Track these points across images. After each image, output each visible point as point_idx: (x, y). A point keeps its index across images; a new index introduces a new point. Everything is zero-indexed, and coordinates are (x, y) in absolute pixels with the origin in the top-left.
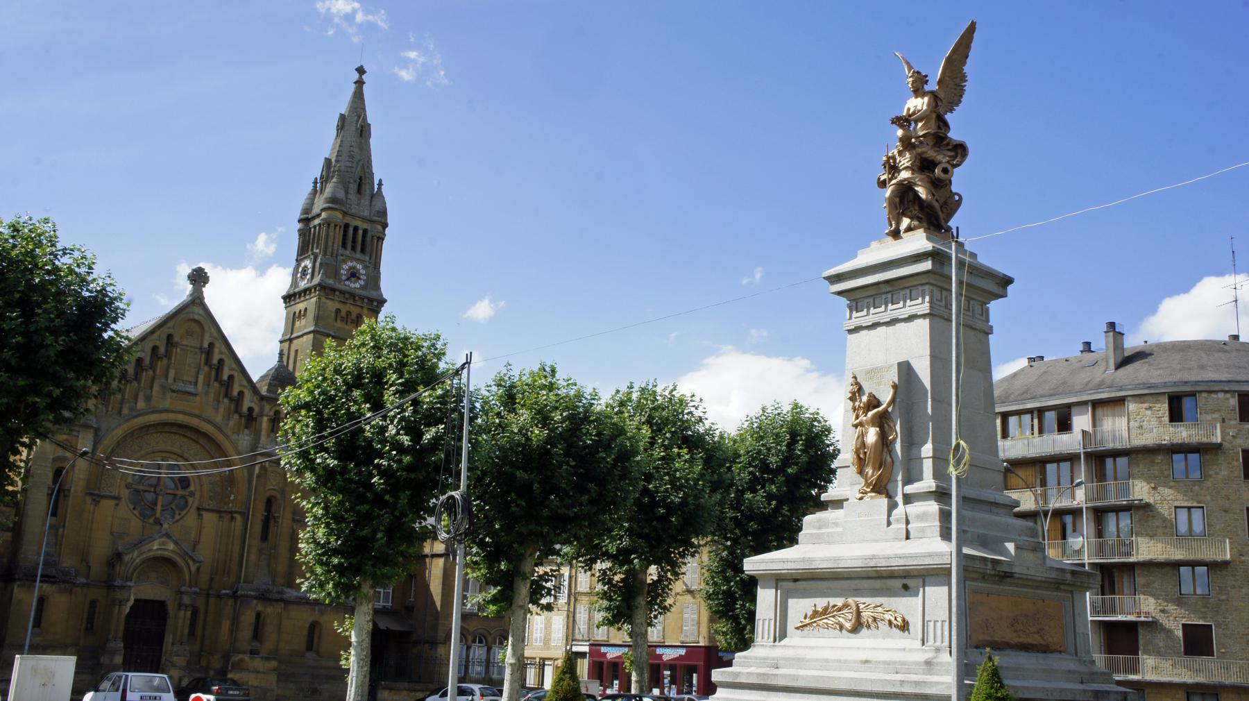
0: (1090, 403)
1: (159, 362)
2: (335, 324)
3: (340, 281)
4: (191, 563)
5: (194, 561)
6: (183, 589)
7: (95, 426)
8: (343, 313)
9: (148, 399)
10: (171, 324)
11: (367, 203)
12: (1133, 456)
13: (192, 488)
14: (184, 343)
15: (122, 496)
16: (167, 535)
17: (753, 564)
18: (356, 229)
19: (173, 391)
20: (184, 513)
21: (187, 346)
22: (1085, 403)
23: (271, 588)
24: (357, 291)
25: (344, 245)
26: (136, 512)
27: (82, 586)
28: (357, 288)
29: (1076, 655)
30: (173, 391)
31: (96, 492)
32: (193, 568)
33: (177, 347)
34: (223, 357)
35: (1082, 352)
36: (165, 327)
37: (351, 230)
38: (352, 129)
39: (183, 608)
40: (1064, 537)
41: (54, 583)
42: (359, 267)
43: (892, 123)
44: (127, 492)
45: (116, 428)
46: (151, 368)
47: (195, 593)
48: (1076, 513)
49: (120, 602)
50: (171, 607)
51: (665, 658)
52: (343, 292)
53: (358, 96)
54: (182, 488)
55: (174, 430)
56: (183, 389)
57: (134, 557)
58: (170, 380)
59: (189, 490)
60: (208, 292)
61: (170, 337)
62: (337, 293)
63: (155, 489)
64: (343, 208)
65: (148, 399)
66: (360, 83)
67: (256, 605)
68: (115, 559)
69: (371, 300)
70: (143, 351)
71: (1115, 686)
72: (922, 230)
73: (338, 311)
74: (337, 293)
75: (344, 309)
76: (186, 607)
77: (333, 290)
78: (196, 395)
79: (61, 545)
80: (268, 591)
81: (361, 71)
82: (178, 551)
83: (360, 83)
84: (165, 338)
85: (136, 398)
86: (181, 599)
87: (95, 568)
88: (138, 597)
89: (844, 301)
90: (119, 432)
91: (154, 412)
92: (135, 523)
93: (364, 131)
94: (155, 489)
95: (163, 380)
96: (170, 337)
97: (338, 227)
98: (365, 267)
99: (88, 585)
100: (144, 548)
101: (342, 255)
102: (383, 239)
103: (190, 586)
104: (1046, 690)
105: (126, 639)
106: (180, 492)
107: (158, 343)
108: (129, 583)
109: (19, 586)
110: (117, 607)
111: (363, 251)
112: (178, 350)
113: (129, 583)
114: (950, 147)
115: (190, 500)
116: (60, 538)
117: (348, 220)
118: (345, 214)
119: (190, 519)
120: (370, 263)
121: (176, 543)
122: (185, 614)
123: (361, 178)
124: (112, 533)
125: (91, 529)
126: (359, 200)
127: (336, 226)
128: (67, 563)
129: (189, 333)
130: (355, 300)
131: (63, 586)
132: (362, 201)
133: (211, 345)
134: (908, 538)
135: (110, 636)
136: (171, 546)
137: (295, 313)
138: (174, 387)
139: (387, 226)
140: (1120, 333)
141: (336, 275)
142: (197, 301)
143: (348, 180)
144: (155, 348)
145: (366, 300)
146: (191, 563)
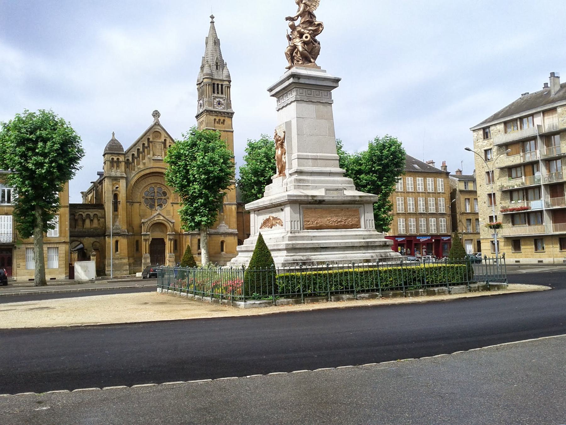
0: (541, 112)
4: (170, 223)
5: (172, 223)
8: (217, 120)
10: (148, 134)
11: (221, 73)
12: (561, 134)
13: (168, 195)
15: (141, 201)
17: (248, 206)
18: (218, 85)
19: (153, 160)
20: (166, 205)
22: (539, 112)
24: (222, 110)
25: (214, 92)
26: (148, 207)
31: (131, 201)
35: (543, 88)
37: (216, 86)
38: (211, 43)
40: (534, 174)
43: (286, 20)
44: (143, 199)
46: (143, 152)
47: (174, 234)
48: (537, 162)
51: (421, 240)
52: (216, 112)
53: (213, 28)
54: (164, 196)
61: (149, 139)
62: (213, 112)
65: (144, 164)
69: (228, 113)
71: (384, 239)
73: (215, 120)
74: (213, 112)
75: (217, 119)
77: (212, 111)
81: (212, 17)
87: (135, 229)
89: (275, 99)
93: (217, 42)
104: (337, 243)
106: (163, 198)
109: (108, 237)
111: (222, 93)
114: (316, 26)
118: (212, 79)
124: (140, 215)
125: (132, 215)
126: (218, 72)
127: (209, 85)
130: (221, 114)
133: (165, 140)
134: (287, 191)
136: (162, 218)
138: (153, 158)
139: (231, 81)
140: (557, 77)
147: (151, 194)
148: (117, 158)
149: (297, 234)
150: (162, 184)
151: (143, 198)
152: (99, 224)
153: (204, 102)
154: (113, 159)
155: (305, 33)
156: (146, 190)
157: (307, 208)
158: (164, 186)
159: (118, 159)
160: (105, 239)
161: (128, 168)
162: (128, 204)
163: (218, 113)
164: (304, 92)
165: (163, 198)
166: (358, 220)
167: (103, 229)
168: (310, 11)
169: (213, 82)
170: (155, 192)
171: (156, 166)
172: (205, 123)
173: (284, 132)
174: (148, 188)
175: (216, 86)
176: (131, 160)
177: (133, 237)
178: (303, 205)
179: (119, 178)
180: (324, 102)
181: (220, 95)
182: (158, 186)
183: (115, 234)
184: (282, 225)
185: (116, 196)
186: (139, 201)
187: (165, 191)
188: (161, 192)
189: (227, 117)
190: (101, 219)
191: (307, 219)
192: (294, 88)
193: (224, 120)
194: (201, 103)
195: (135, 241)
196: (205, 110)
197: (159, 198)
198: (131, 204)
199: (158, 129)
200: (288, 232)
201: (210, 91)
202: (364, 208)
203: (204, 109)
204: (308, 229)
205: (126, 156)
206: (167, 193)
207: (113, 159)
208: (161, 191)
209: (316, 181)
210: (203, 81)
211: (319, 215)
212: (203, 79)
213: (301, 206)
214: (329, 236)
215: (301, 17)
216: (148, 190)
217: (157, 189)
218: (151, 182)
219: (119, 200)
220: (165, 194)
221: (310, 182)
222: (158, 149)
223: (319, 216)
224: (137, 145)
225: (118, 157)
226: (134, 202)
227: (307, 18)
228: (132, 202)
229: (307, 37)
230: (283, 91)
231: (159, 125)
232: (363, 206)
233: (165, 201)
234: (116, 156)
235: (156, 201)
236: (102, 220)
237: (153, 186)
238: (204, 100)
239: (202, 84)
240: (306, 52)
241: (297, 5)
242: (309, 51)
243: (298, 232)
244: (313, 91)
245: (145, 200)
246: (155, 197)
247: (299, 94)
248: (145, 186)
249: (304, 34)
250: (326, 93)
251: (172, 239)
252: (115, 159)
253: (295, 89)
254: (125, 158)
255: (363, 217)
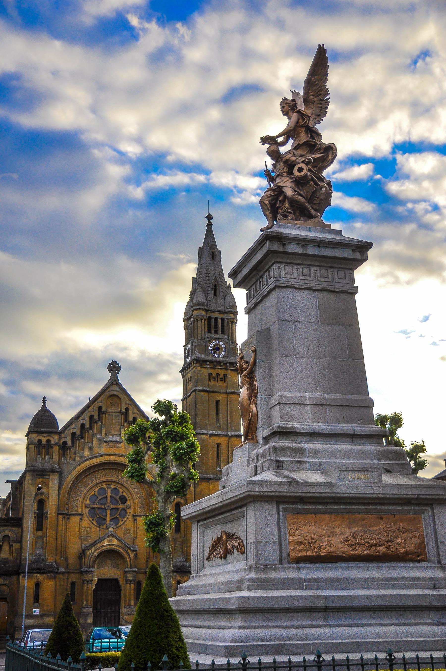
1: (95, 425)
2: (210, 383)
3: (209, 355)
4: (130, 552)
5: (132, 551)
6: (126, 569)
7: (59, 470)
8: (214, 375)
9: (91, 449)
13: (128, 503)
14: (110, 411)
15: (84, 513)
16: (112, 535)
19: (106, 442)
20: (124, 520)
21: (112, 412)
23: (185, 564)
24: (221, 359)
25: (209, 331)
26: (94, 522)
27: (63, 573)
28: (222, 358)
29: (439, 562)
30: (106, 442)
31: (66, 512)
32: (132, 556)
33: (105, 414)
34: (135, 415)
36: (96, 402)
37: (213, 320)
38: (206, 255)
39: (128, 582)
41: (44, 573)
42: (221, 343)
44: (87, 510)
45: (73, 470)
47: (135, 572)
49: (88, 582)
50: (121, 582)
52: (211, 362)
53: (210, 234)
55: (111, 467)
56: (112, 440)
57: (93, 552)
58: (103, 435)
59: (126, 504)
60: (120, 376)
61: (100, 408)
62: (208, 363)
63: (105, 506)
64: (205, 307)
65: (91, 449)
66: (209, 225)
67: (176, 576)
68: (83, 553)
70: (84, 419)
72: (290, 196)
73: (210, 374)
74: (208, 363)
75: (214, 372)
76: (131, 582)
77: (205, 361)
78: (121, 442)
79: (46, 548)
80: (183, 566)
82: (121, 545)
83: (209, 225)
84: (97, 409)
85: (83, 449)
86: (126, 576)
87: (71, 561)
88: (100, 578)
90: (75, 473)
91: (95, 457)
92: (95, 529)
94: (105, 506)
95: (98, 436)
96: (100, 408)
97: (203, 320)
98: (225, 343)
99: (68, 573)
100: (99, 545)
101: (208, 338)
102: (236, 323)
103: (131, 567)
105: (95, 607)
106: (121, 506)
107: (93, 413)
108: (92, 569)
110: (86, 585)
112: (107, 416)
113: (92, 569)
114: (322, 151)
115: (128, 511)
116: (44, 544)
117: (209, 314)
118: (207, 311)
119: (129, 524)
120: (228, 340)
121: (118, 540)
122: (130, 586)
123: (215, 286)
124: (80, 538)
126: (216, 300)
127: (202, 320)
128: (51, 559)
129: (113, 404)
130: (221, 366)
131: (49, 575)
132: (218, 301)
133: (127, 409)
135: (84, 605)
136: (116, 542)
137: (187, 380)
141: (205, 351)
142: (114, 383)
143: (207, 289)
144: (91, 417)
145: (228, 364)
146: (130, 552)
147: (100, 500)
148: (46, 439)
149: (273, 575)
150: (119, 483)
151: (87, 506)
152: (11, 552)
153: (194, 346)
154: (40, 441)
155: (298, 163)
156: (93, 493)
157: (297, 512)
158: (122, 487)
159: (48, 441)
160: (18, 579)
161: (64, 455)
162: (61, 517)
163: (215, 363)
164: (295, 271)
165: (121, 506)
166: (419, 541)
167: (18, 561)
168: (310, 125)
169: (208, 316)
170: (107, 497)
171: (110, 452)
172: (194, 381)
173: (255, 351)
174: (96, 490)
175: (213, 320)
176: (69, 442)
177: (66, 576)
178: (286, 506)
179: (48, 473)
180: (338, 290)
181: (220, 336)
182: (113, 487)
183: (33, 570)
184: (243, 553)
185: (41, 504)
186: (79, 512)
187: (124, 494)
188: (117, 498)
189: (231, 370)
190: (14, 544)
191: (296, 538)
192: (273, 264)
193: (225, 376)
194: (189, 349)
195: (69, 583)
196: (195, 359)
197: (114, 507)
198: (66, 517)
199: (115, 390)
200: (250, 568)
201: (204, 329)
202: (433, 513)
203: (194, 357)
204: (299, 560)
205: (63, 436)
206: (127, 497)
207: (40, 441)
208: (117, 495)
209: (320, 452)
210: (192, 315)
211: (324, 529)
212: (193, 311)
213: (281, 506)
214: (348, 580)
215: (292, 139)
216: (96, 494)
217: (112, 492)
218: (102, 480)
219: (45, 512)
220: (123, 500)
221: (307, 454)
222: (115, 424)
223: (324, 532)
224: (81, 418)
225: (49, 438)
226: (71, 515)
227: (304, 137)
228: (67, 514)
229: (300, 170)
230: (254, 272)
231: (118, 384)
232: (429, 508)
233: (123, 512)
234: (44, 437)
235: (108, 512)
236: (16, 546)
237: (105, 487)
238: (194, 343)
239: (192, 319)
240: (300, 197)
241: (285, 117)
242: (309, 197)
243: (275, 569)
244: (313, 269)
245: (89, 510)
246: (106, 506)
247: (284, 275)
248: (90, 486)
249: (295, 165)
250: (341, 273)
251: (132, 580)
252: (44, 440)
253: (274, 266)
254: (60, 439)
255: (78, 444)
